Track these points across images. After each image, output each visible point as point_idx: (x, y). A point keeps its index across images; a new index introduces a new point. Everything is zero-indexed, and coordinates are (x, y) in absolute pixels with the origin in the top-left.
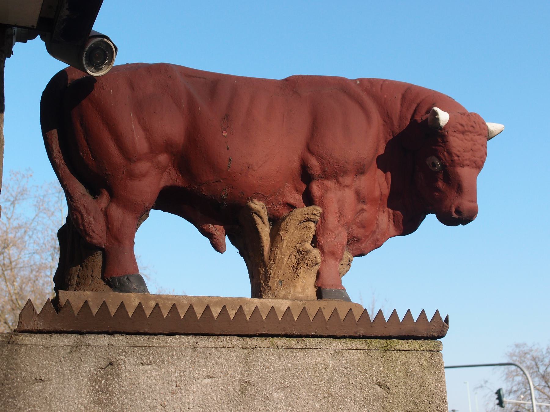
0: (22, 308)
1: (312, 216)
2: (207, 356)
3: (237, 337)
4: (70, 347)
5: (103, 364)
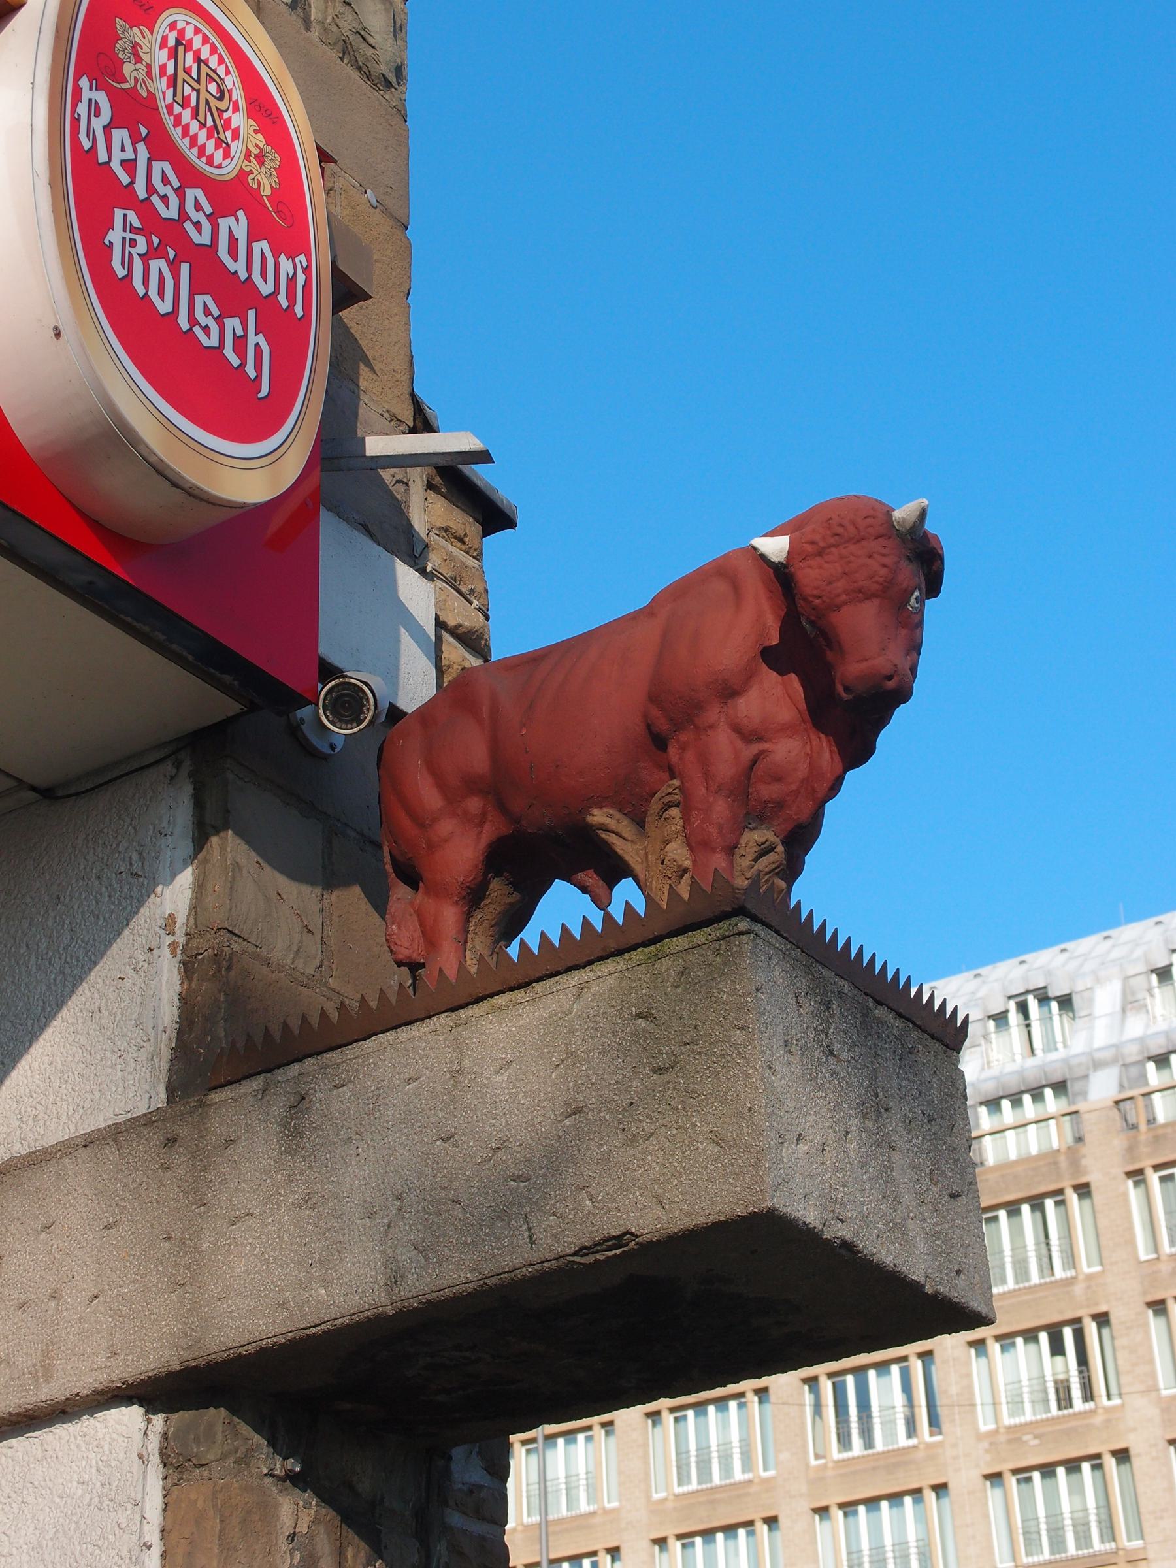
0: (1017, 1134)
1: (669, 798)
2: (408, 1051)
3: (446, 1014)
4: (260, 1092)
5: (293, 1100)
